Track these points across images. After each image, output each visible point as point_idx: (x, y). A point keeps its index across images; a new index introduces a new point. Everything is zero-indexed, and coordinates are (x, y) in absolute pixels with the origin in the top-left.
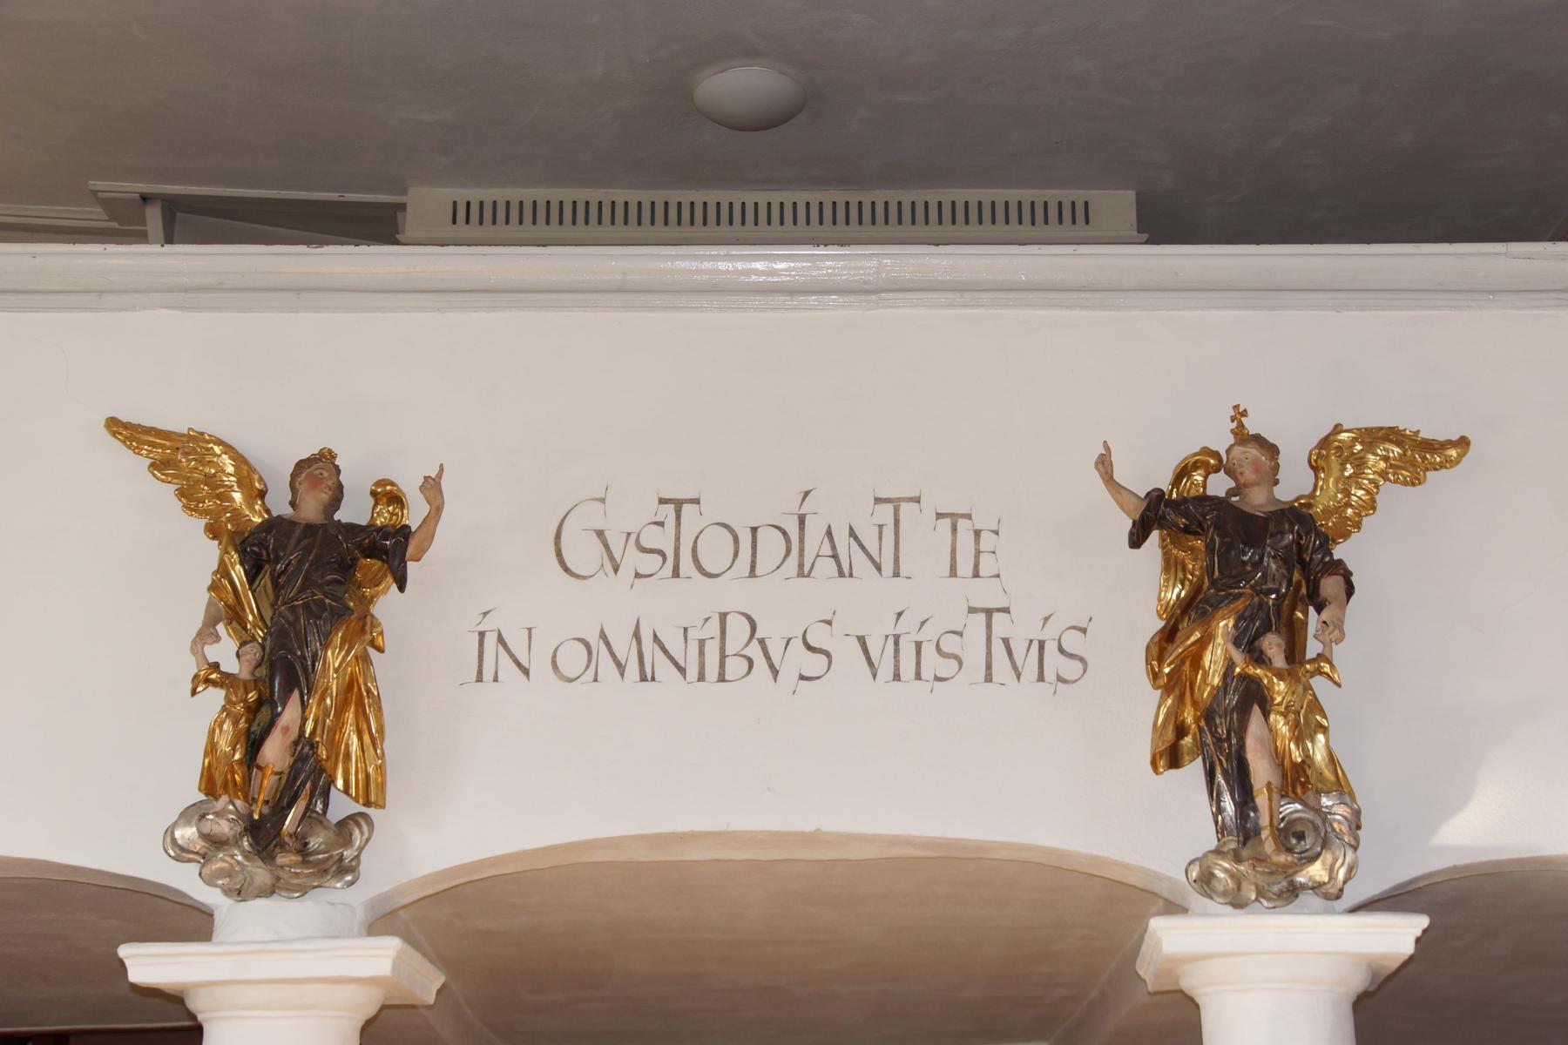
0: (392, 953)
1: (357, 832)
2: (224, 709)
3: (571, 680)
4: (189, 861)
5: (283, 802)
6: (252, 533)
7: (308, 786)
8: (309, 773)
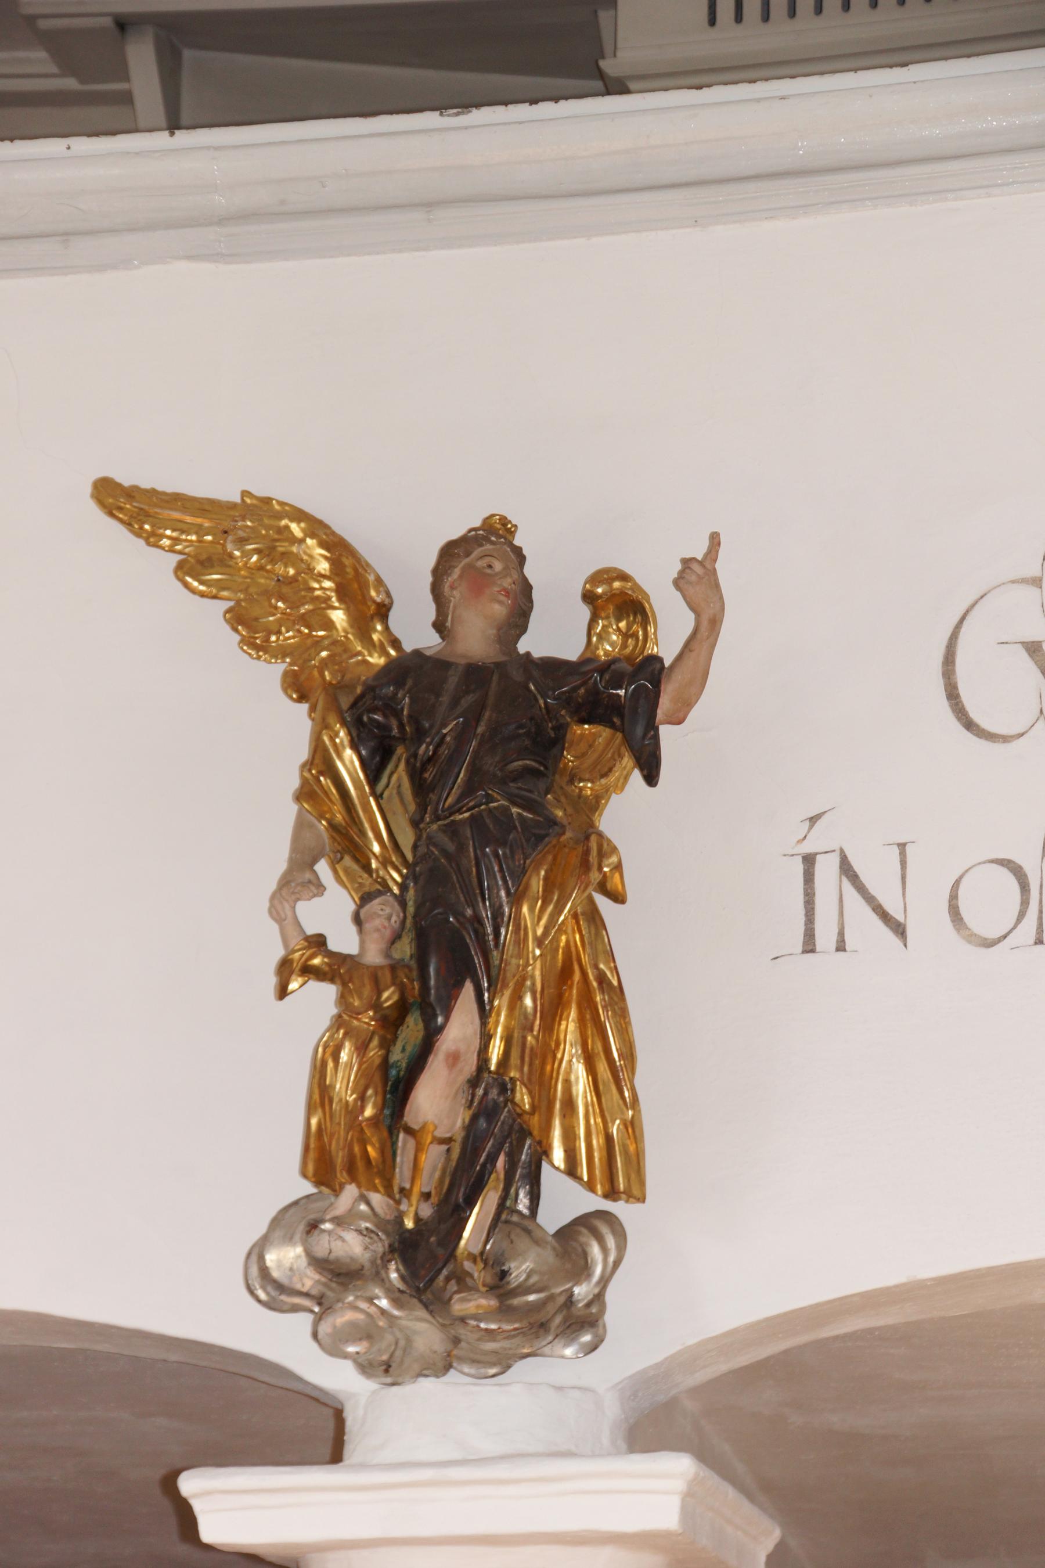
0: (679, 1485)
1: (595, 1250)
2: (338, 1022)
3: (990, 944)
4: (295, 1309)
5: (457, 1188)
6: (370, 689)
7: (501, 1162)
8: (500, 1141)
